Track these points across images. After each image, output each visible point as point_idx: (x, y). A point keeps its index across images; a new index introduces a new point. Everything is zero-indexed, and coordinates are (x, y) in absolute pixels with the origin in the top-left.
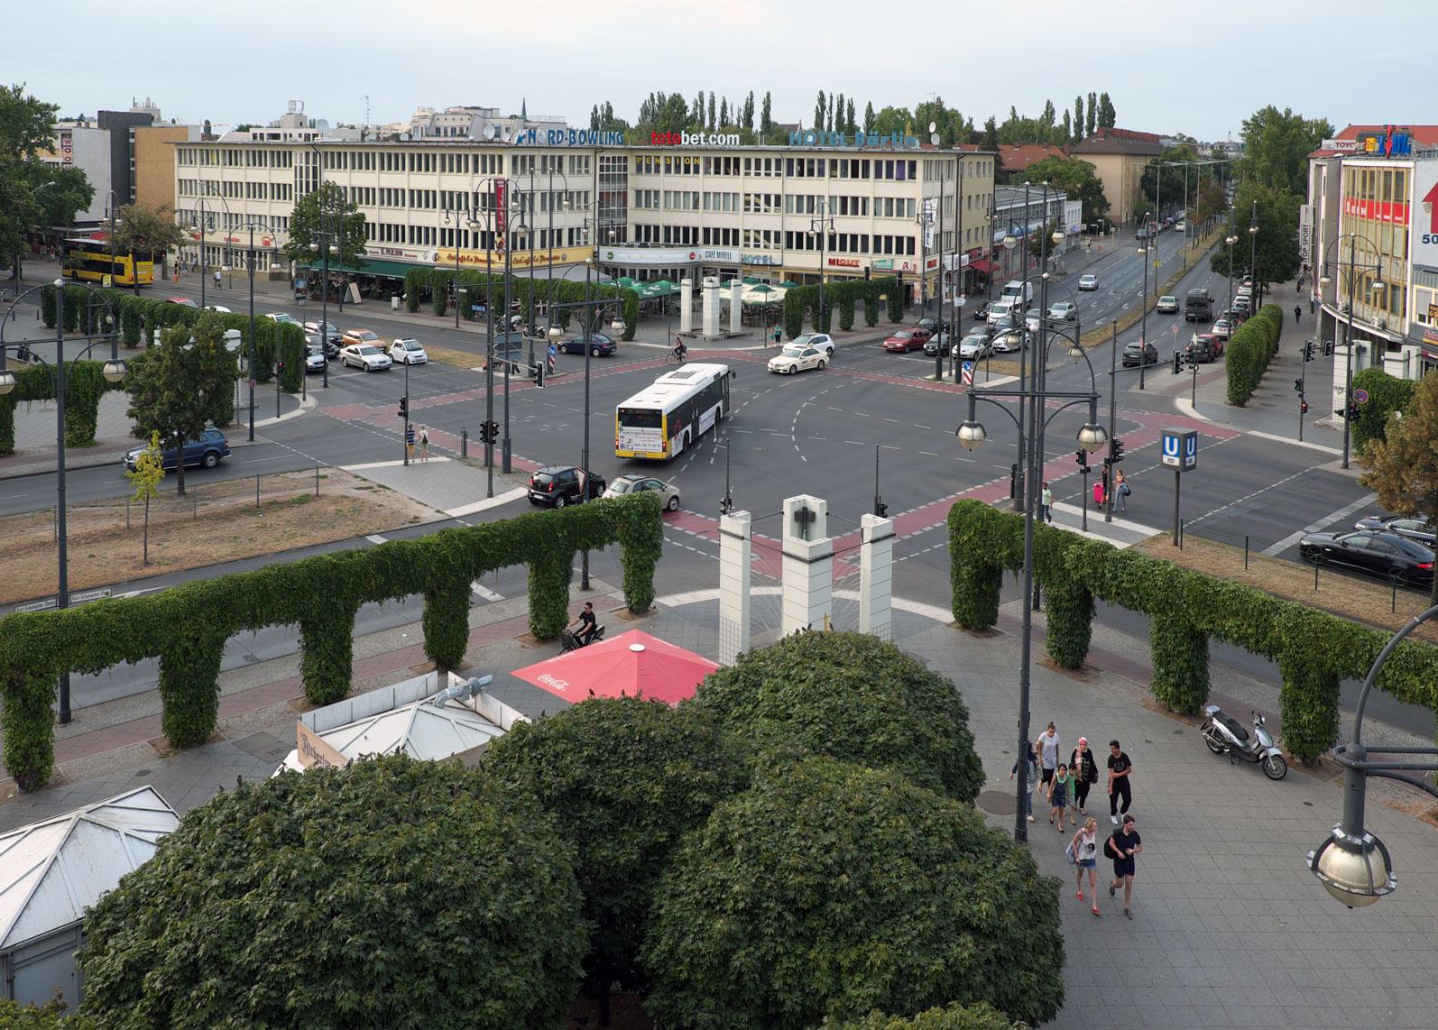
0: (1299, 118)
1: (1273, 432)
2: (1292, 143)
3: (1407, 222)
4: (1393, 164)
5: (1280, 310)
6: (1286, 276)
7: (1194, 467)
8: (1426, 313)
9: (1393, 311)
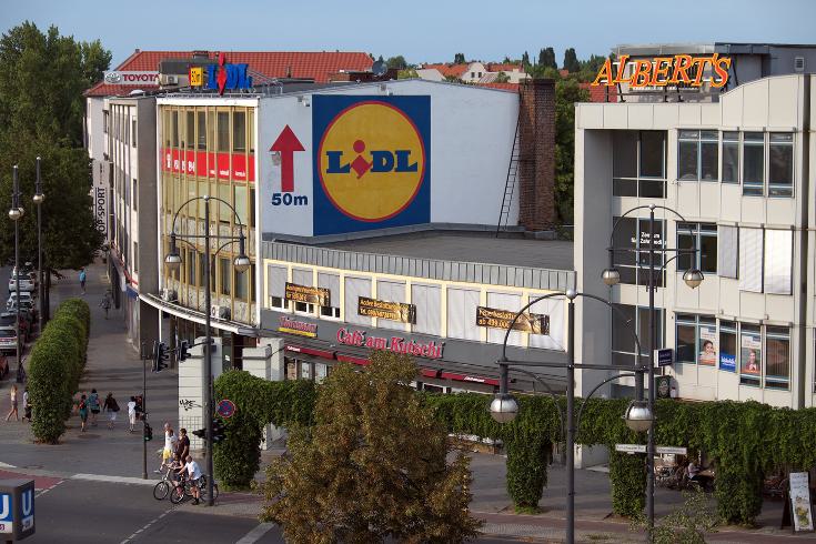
0: (70, 41)
1: (102, 473)
2: (61, 76)
3: (252, 178)
4: (231, 102)
5: (85, 307)
6: (84, 259)
7: (32, 531)
8: (281, 294)
9: (238, 295)
